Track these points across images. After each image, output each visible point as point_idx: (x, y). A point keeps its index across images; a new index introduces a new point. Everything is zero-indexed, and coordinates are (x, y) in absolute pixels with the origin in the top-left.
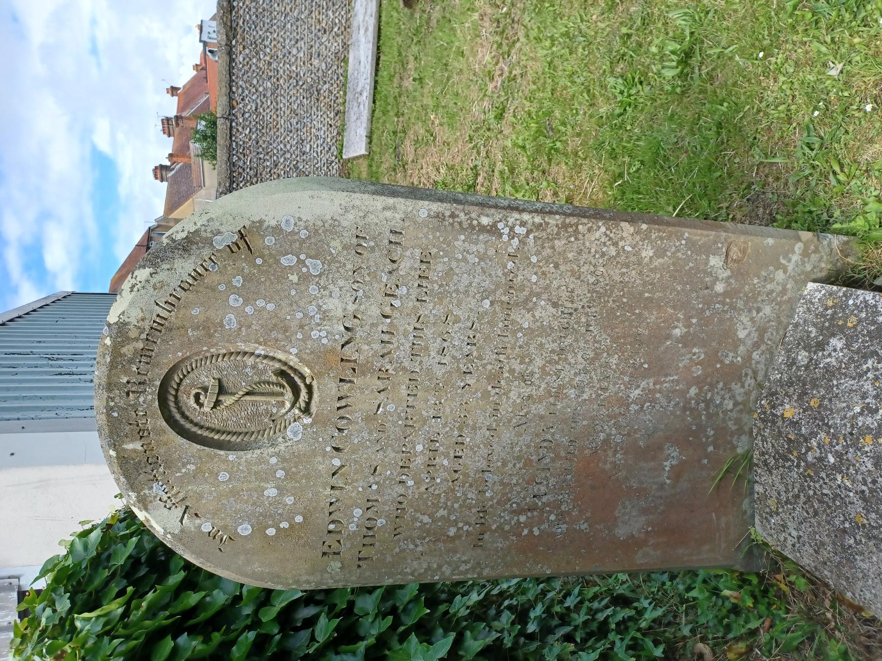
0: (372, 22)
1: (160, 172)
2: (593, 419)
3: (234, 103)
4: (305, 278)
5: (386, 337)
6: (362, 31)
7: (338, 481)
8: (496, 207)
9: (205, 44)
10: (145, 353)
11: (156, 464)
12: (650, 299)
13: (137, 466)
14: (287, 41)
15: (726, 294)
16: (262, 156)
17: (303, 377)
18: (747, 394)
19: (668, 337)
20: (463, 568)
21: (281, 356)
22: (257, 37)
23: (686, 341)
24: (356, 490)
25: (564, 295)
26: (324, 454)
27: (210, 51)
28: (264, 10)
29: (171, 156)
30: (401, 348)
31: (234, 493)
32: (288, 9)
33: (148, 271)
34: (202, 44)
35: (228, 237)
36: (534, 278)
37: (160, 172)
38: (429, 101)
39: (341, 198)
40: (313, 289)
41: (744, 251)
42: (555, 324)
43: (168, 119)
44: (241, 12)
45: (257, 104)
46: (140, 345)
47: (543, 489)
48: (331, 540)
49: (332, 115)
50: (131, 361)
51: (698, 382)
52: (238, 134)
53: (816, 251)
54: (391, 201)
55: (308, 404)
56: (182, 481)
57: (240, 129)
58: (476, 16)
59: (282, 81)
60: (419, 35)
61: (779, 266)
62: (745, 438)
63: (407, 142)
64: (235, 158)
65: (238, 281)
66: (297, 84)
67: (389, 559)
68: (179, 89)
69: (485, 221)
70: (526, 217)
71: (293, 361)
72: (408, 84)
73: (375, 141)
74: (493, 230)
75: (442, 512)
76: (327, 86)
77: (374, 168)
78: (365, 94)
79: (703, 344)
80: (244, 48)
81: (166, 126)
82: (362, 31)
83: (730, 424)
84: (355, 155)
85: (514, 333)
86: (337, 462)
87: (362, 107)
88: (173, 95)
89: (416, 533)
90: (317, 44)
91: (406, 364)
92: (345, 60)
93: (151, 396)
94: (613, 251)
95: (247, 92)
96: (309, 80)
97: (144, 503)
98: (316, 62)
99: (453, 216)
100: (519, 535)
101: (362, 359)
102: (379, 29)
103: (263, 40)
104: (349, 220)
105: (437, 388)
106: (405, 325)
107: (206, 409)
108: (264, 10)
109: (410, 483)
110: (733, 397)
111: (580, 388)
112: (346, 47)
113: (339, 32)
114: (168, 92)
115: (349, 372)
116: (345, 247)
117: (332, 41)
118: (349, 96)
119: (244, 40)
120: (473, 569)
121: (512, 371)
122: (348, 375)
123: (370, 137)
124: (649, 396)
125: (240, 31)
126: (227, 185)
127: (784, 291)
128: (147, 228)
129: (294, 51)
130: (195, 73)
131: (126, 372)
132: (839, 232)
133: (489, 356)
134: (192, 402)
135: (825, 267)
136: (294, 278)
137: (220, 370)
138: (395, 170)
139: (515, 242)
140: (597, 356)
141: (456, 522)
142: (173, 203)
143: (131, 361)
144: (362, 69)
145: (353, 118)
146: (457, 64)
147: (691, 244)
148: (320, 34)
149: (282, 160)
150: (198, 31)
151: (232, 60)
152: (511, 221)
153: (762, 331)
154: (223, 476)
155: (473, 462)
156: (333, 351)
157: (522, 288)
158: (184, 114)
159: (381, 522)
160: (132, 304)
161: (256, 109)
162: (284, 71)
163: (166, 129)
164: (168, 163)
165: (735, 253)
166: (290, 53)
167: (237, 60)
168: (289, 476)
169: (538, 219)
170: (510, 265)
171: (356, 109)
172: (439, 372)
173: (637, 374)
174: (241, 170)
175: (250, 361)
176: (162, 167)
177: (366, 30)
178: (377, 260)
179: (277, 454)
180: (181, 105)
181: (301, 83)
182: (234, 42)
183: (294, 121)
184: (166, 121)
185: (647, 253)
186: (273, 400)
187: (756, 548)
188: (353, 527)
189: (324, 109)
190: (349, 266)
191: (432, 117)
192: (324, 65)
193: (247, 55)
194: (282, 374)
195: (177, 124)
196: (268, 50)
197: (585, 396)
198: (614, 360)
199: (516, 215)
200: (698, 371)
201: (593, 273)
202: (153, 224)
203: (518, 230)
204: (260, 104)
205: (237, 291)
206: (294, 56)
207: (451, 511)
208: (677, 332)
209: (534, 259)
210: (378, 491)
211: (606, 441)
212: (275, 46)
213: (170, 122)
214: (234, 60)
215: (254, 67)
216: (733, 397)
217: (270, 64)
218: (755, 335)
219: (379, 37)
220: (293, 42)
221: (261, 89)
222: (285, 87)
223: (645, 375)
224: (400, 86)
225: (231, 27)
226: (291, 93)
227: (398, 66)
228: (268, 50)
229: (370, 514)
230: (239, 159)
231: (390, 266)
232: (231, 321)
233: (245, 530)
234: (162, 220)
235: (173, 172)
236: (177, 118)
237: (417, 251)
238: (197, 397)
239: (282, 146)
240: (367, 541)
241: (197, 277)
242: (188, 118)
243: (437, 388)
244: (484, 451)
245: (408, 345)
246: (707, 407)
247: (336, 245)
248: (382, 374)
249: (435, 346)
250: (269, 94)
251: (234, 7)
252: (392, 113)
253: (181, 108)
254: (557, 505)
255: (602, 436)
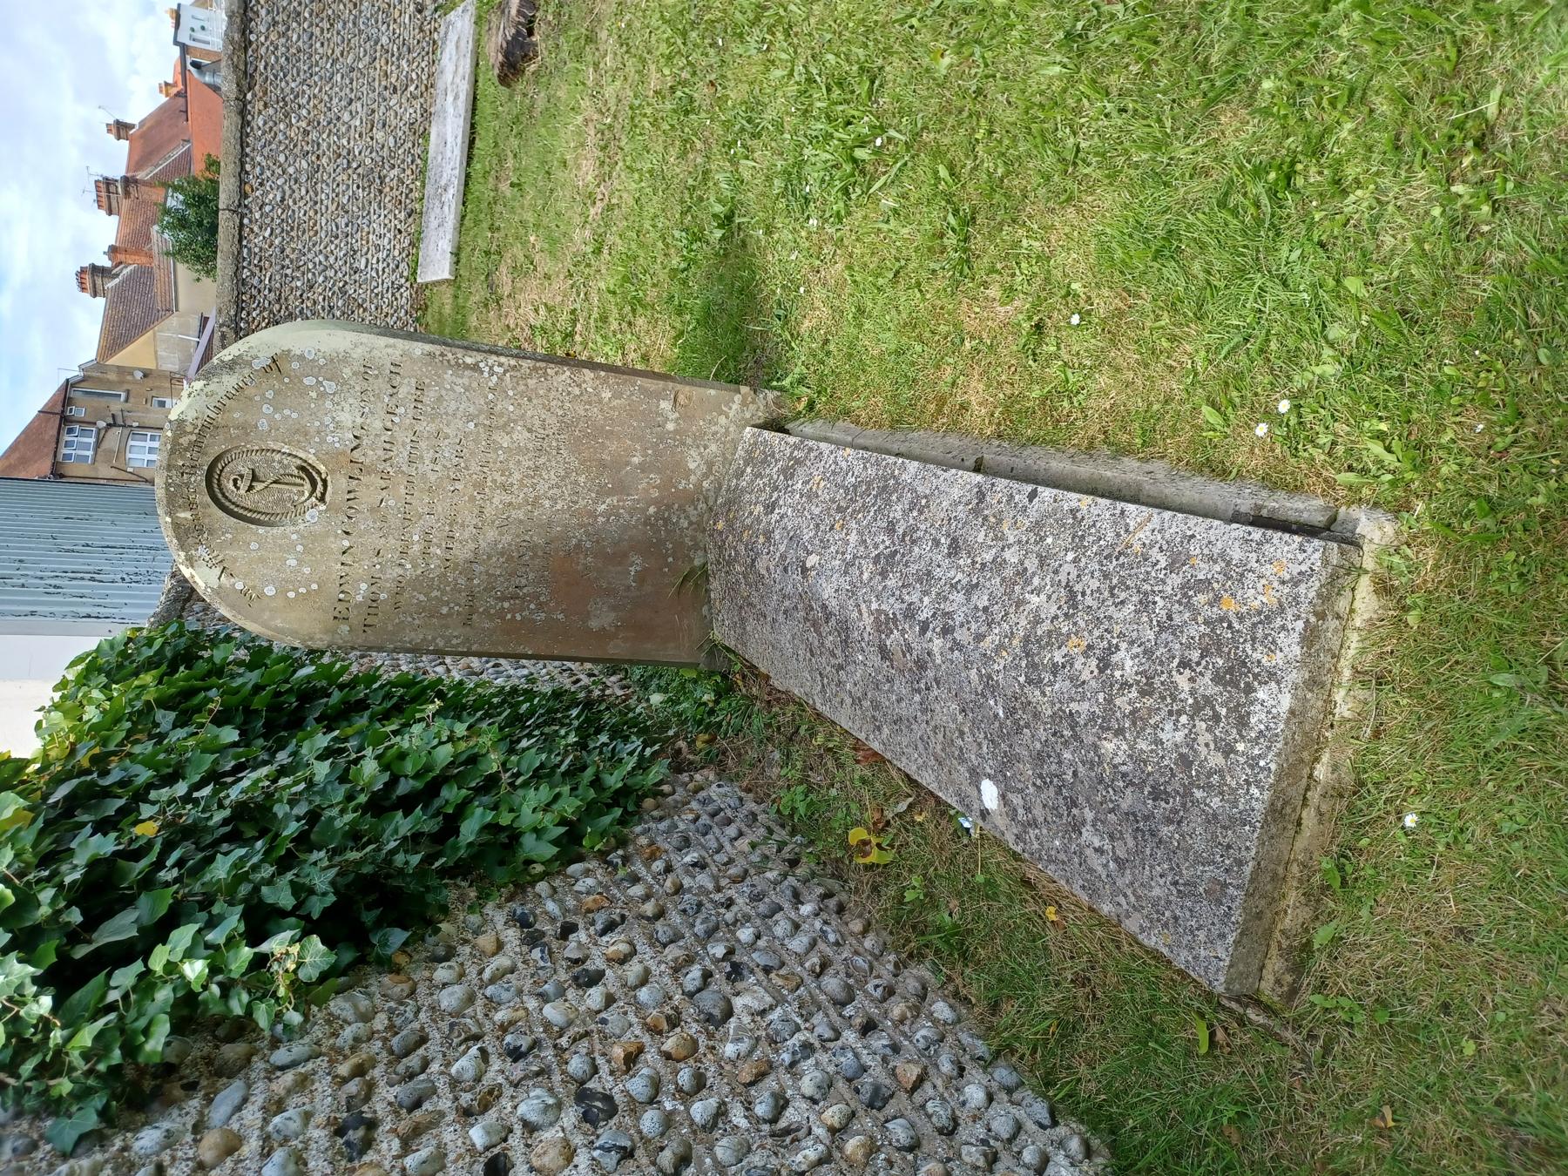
0: (464, 87)
1: (91, 278)
2: (565, 526)
3: (247, 188)
4: (322, 395)
5: (388, 446)
6: (450, 98)
7: (347, 559)
8: (478, 350)
9: (185, 49)
10: (196, 444)
11: (201, 532)
12: (612, 432)
13: (187, 532)
14: (335, 101)
15: (676, 432)
16: (289, 272)
17: (319, 473)
18: (701, 515)
19: (628, 463)
20: (454, 642)
21: (302, 454)
22: (287, 90)
23: (643, 467)
24: (362, 568)
25: (537, 423)
26: (336, 535)
27: (196, 65)
28: (299, 51)
29: (113, 250)
30: (401, 455)
31: (262, 560)
32: (338, 52)
33: (202, 383)
34: (177, 50)
35: (263, 361)
36: (511, 408)
37: (91, 278)
38: (530, 217)
39: (352, 337)
40: (328, 404)
41: (689, 399)
42: (530, 446)
43: (108, 182)
44: (262, 51)
45: (284, 192)
46: (194, 438)
47: (524, 581)
48: (340, 607)
49: (402, 216)
50: (186, 450)
51: (655, 502)
52: (252, 236)
53: (753, 402)
54: (392, 341)
55: (323, 494)
56: (221, 547)
57: (256, 229)
58: (580, 119)
59: (324, 160)
60: (519, 123)
61: (721, 413)
62: (700, 553)
63: (503, 269)
64: (246, 273)
65: (270, 394)
66: (349, 167)
67: (390, 628)
68: (132, 126)
69: (469, 360)
70: (503, 359)
71: (312, 459)
72: (504, 187)
73: (463, 261)
74: (475, 367)
75: (435, 593)
76: (395, 172)
77: (461, 301)
78: (451, 191)
79: (659, 471)
80: (266, 105)
81: (103, 194)
82: (450, 98)
83: (687, 540)
84: (435, 278)
85: (496, 450)
86: (346, 543)
87: (446, 208)
88: (119, 138)
89: (413, 609)
90: (382, 109)
91: (404, 468)
92: (425, 135)
93: (199, 478)
94: (577, 391)
95: (268, 173)
96: (368, 161)
97: (191, 561)
98: (379, 135)
99: (442, 355)
100: (503, 619)
101: (367, 461)
102: (475, 98)
103: (297, 97)
104: (357, 353)
105: (430, 490)
106: (404, 437)
107: (242, 492)
108: (299, 51)
109: (409, 566)
110: (687, 517)
111: (554, 500)
112: (427, 115)
113: (417, 93)
114: (109, 131)
115: (357, 471)
116: (354, 374)
117: (405, 104)
118: (429, 190)
119: (265, 93)
120: (463, 643)
121: (494, 481)
122: (356, 473)
123: (457, 254)
124: (612, 511)
125: (259, 80)
126: (232, 313)
127: (727, 433)
128: (62, 381)
129: (346, 117)
130: (163, 99)
131: (182, 457)
132: (775, 388)
133: (475, 468)
134: (231, 486)
135: (762, 416)
136: (314, 395)
137: (253, 462)
138: (486, 306)
139: (495, 379)
140: (567, 475)
141: (447, 603)
142: (117, 335)
143: (186, 450)
144: (449, 154)
145: (434, 223)
146: (560, 175)
147: (642, 390)
148: (387, 94)
149: (321, 279)
150: (170, 22)
151: (245, 123)
152: (490, 362)
153: (710, 465)
154: (254, 546)
155: (462, 553)
156: (343, 453)
157: (501, 415)
158: (140, 175)
159: (383, 596)
160: (189, 406)
161: (283, 200)
162: (329, 146)
163: (104, 200)
164: (107, 263)
165: (681, 398)
166: (338, 119)
167: (253, 124)
168: (307, 551)
169: (513, 362)
170: (491, 396)
171: (437, 210)
172: (433, 477)
173: (602, 492)
174: (254, 292)
175: (277, 457)
176: (95, 270)
177: (456, 98)
178: (381, 385)
179: (297, 532)
180: (136, 158)
181: (354, 165)
182: (249, 96)
183: (342, 222)
184: (106, 186)
185: (606, 395)
186: (295, 489)
187: (715, 649)
188: (359, 598)
189: (389, 206)
190: (358, 388)
191: (532, 239)
192: (391, 140)
193: (270, 117)
194: (302, 468)
195: (127, 194)
196: (304, 112)
197: (559, 507)
198: (582, 479)
199: (494, 358)
200: (655, 494)
201: (561, 407)
202: (74, 373)
203: (496, 369)
204: (288, 193)
205: (269, 402)
206: (344, 123)
207: (444, 593)
208: (636, 460)
209: (511, 393)
210: (381, 571)
211: (578, 546)
212: (315, 106)
213: (112, 189)
214: (249, 123)
215: (280, 137)
216: (687, 517)
217: (306, 133)
218: (704, 468)
219: (474, 109)
220: (343, 103)
221: (291, 170)
222: (330, 169)
223: (610, 493)
224: (496, 190)
225: (245, 72)
226: (339, 179)
227: (495, 160)
228: (304, 112)
229: (374, 589)
230: (253, 274)
231: (391, 391)
232: (263, 424)
233: (270, 591)
234: (92, 368)
235: (117, 281)
236: (128, 181)
237: (413, 381)
238: (235, 481)
239: (321, 258)
240: (371, 611)
241: (239, 389)
242: (145, 183)
243: (430, 490)
244: (472, 546)
245: (406, 454)
246: (665, 525)
247: (347, 372)
248: (384, 475)
249: (428, 456)
250: (303, 179)
251: (251, 43)
252: (485, 225)
253: (137, 162)
254: (536, 596)
255: (574, 541)
